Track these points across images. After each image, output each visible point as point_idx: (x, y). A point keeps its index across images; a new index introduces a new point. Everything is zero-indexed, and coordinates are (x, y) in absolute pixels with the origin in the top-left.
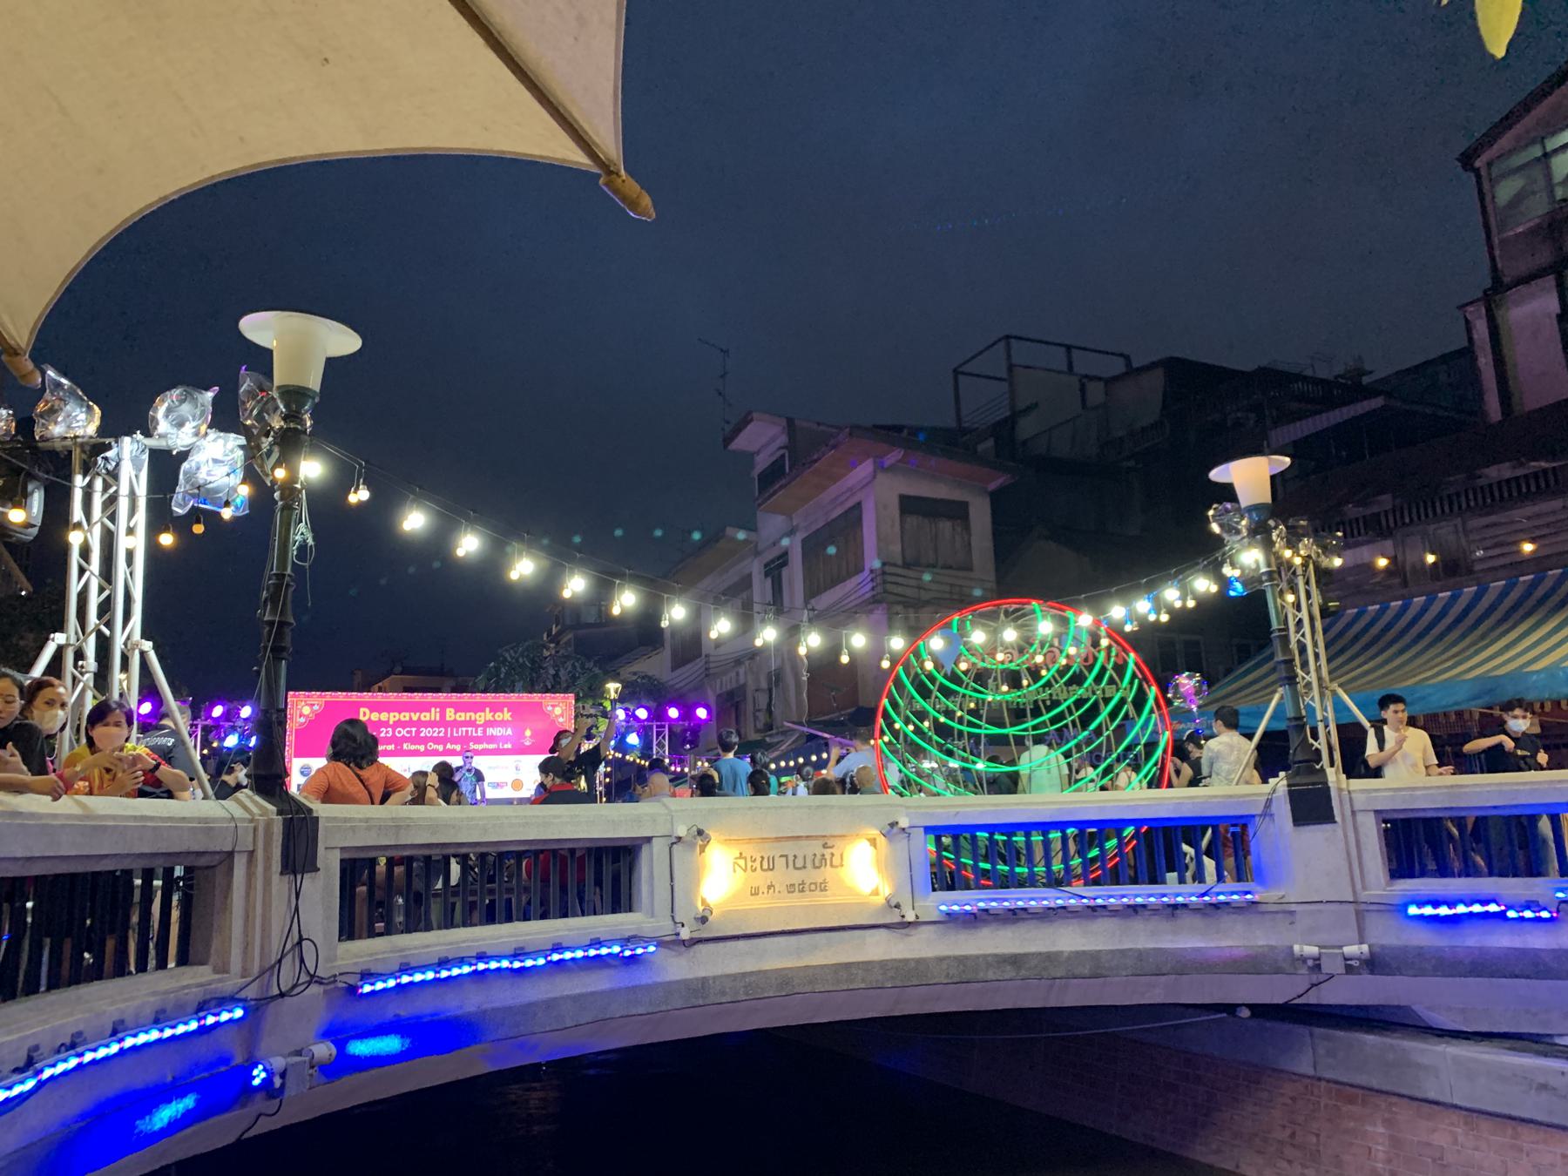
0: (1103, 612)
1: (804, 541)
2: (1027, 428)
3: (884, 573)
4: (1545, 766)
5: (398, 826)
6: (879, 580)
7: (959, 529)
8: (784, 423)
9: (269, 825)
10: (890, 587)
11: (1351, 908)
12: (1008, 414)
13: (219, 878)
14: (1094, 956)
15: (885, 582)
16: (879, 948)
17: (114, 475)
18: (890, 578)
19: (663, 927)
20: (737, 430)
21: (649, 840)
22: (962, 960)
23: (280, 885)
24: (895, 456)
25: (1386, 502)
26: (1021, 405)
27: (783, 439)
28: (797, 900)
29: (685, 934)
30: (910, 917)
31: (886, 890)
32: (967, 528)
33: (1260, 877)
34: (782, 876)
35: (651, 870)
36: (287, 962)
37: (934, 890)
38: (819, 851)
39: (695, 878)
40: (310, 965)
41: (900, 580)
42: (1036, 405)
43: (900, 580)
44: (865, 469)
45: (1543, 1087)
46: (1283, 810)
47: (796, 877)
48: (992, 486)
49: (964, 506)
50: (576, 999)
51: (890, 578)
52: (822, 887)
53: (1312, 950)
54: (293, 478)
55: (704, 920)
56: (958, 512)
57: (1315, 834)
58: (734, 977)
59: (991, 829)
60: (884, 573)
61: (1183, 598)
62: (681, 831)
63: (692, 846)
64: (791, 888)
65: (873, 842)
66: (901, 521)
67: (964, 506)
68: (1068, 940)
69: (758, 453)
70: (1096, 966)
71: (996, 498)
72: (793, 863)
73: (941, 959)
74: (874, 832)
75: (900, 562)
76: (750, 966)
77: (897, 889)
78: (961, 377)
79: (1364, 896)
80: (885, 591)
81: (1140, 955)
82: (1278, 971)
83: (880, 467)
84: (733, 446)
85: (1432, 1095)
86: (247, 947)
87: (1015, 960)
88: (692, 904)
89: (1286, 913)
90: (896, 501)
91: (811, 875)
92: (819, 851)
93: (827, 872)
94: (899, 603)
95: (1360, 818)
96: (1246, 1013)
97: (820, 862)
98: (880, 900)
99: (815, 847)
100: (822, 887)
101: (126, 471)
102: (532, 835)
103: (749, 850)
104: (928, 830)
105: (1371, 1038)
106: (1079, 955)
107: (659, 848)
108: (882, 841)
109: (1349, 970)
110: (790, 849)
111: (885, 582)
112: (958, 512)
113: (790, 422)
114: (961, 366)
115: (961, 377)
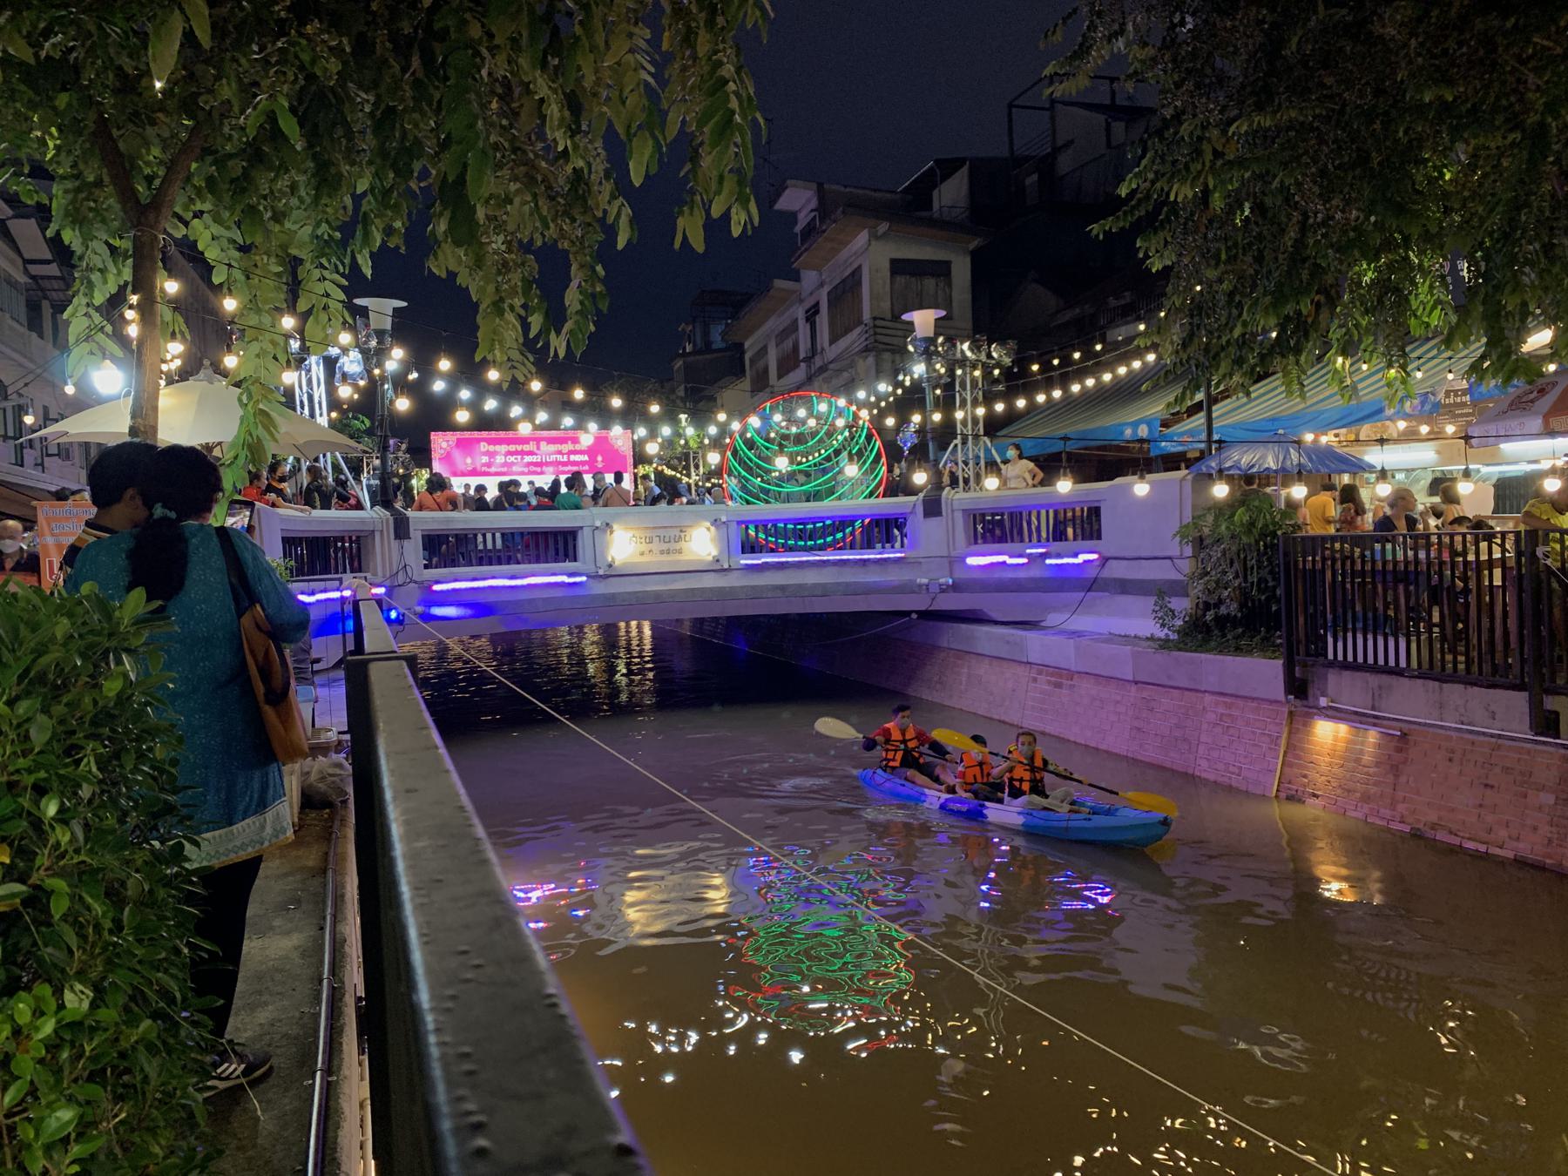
0: (703, 429)
1: (829, 293)
2: (1065, 163)
3: (875, 326)
4: (491, 505)
5: (448, 520)
6: (872, 332)
7: (941, 285)
8: (815, 186)
9: (387, 520)
10: (879, 338)
11: (945, 560)
12: (1049, 150)
13: (370, 541)
14: (824, 586)
15: (875, 334)
16: (710, 581)
17: (309, 371)
18: (879, 330)
19: (591, 569)
20: (778, 195)
21: (581, 528)
22: (753, 587)
23: (395, 544)
24: (883, 227)
25: (1128, 297)
26: (1060, 143)
27: (814, 204)
28: (665, 558)
29: (601, 572)
30: (726, 566)
31: (715, 552)
32: (950, 285)
33: (912, 546)
34: (656, 546)
35: (584, 542)
36: (400, 573)
37: (743, 552)
38: (678, 534)
39: (606, 547)
40: (410, 575)
41: (889, 332)
42: (1072, 142)
43: (889, 332)
44: (863, 237)
45: (1008, 642)
46: (920, 510)
47: (665, 547)
48: (972, 246)
49: (948, 264)
50: (544, 600)
51: (879, 330)
52: (680, 551)
53: (925, 581)
54: (383, 371)
55: (610, 566)
56: (941, 270)
57: (934, 521)
58: (629, 593)
59: (786, 522)
60: (875, 326)
61: (868, 396)
62: (598, 524)
63: (605, 531)
64: (662, 552)
65: (708, 529)
66: (891, 283)
67: (948, 264)
68: (811, 578)
69: (800, 210)
70: (824, 591)
71: (975, 255)
72: (663, 540)
73: (742, 587)
74: (708, 524)
75: (889, 316)
76: (639, 588)
77: (721, 553)
78: (1014, 110)
79: (953, 554)
80: (876, 341)
81: (847, 585)
82: (914, 592)
83: (874, 236)
84: (778, 207)
85: (979, 651)
86: (384, 567)
87: (783, 588)
88: (605, 558)
89: (917, 563)
90: (887, 265)
91: (673, 546)
92: (678, 534)
93: (683, 544)
94: (887, 350)
95: (956, 514)
96: (914, 616)
97: (678, 539)
98: (710, 558)
99: (676, 532)
100: (680, 551)
101: (314, 368)
102: (517, 525)
103: (638, 534)
104: (739, 523)
105: (963, 626)
106: (815, 586)
107: (586, 533)
108: (713, 528)
109: (943, 591)
110: (661, 533)
111: (875, 334)
112: (941, 270)
113: (820, 185)
114: (1016, 98)
115: (1014, 110)
